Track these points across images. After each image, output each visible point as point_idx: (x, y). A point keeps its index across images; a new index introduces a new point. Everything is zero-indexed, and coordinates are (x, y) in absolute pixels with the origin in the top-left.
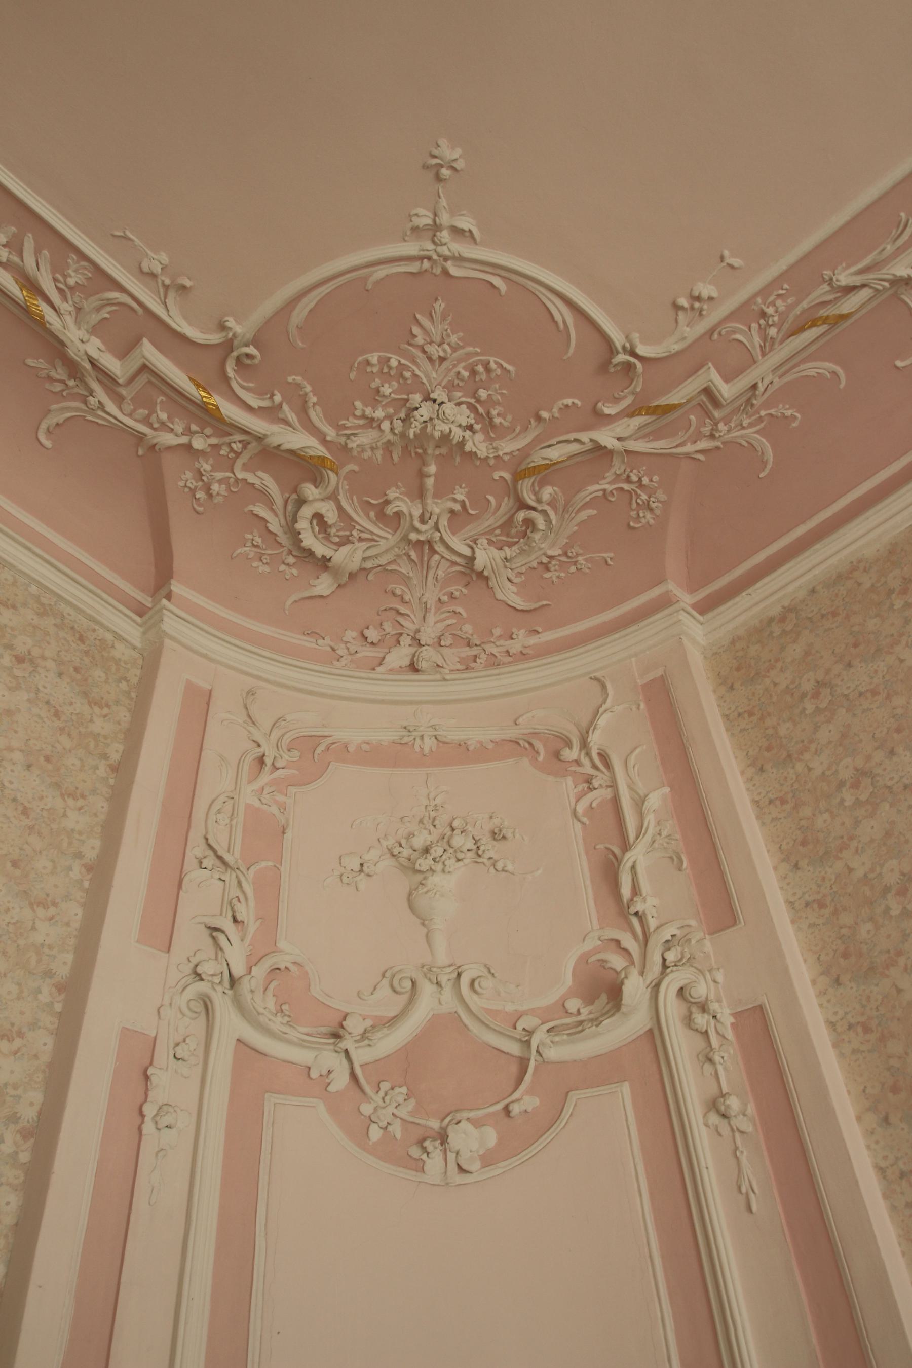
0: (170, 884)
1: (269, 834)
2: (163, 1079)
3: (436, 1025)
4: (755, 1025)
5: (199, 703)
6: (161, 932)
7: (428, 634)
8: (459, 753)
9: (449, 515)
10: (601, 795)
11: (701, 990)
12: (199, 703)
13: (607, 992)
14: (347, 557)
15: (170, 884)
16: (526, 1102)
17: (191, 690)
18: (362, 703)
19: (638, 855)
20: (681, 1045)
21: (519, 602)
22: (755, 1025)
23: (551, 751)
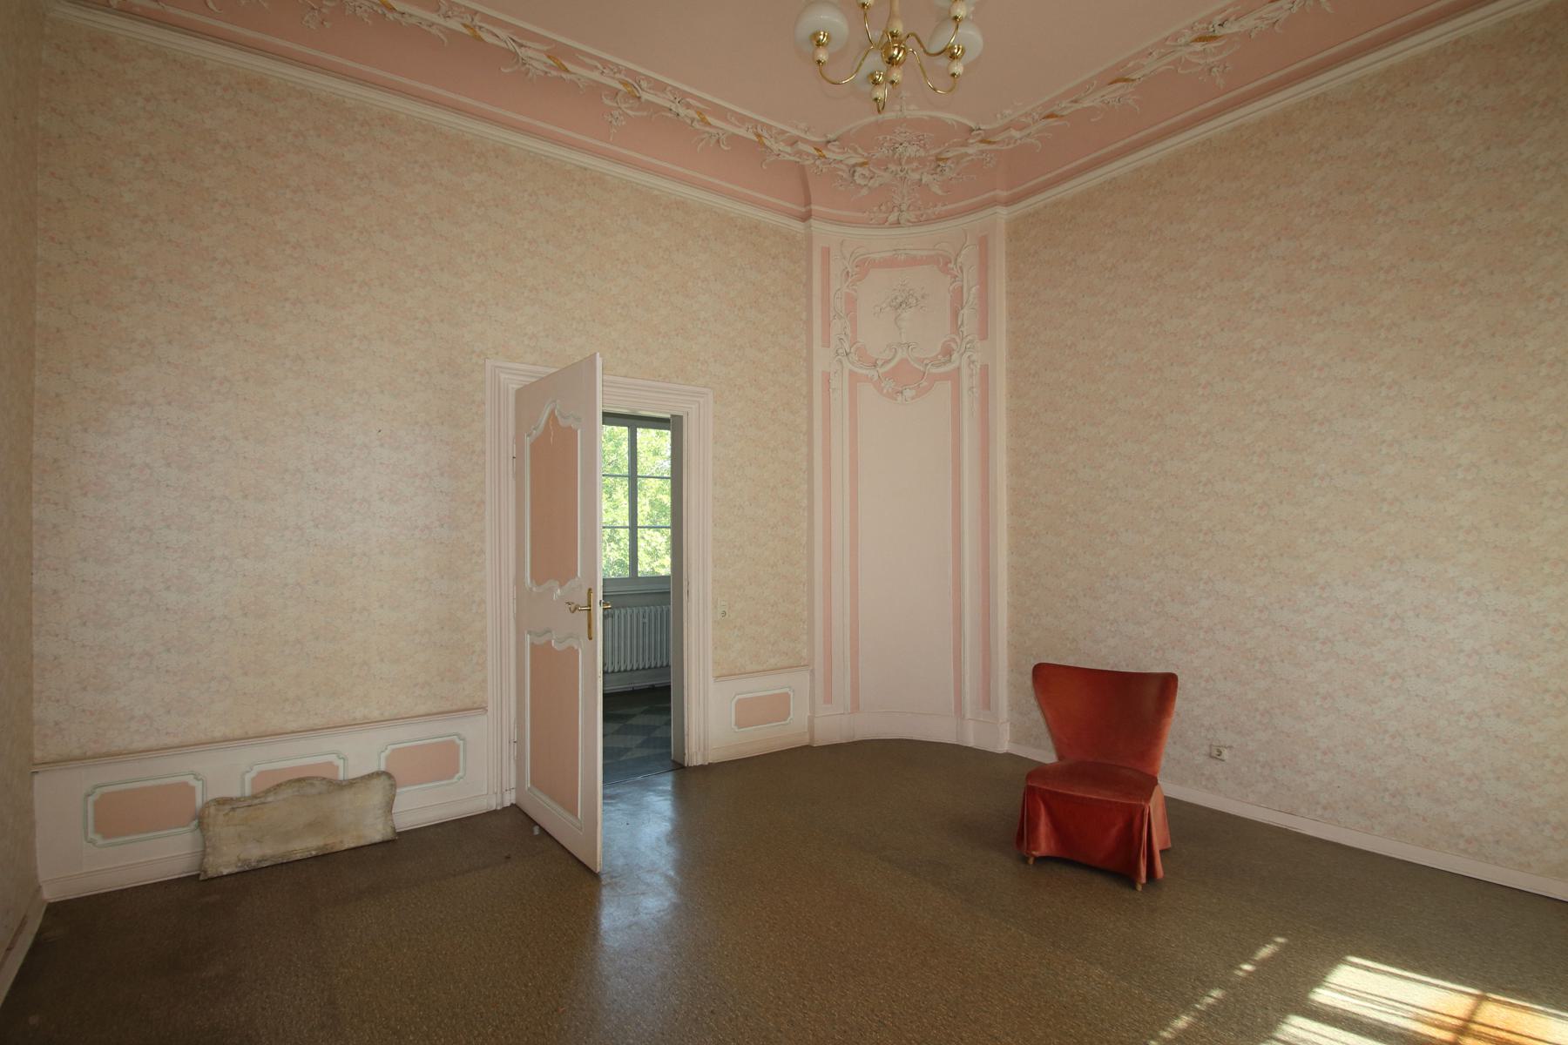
0: (827, 325)
1: (851, 302)
2: (834, 384)
3: (904, 361)
4: (985, 371)
5: (826, 252)
6: (826, 343)
7: (904, 207)
8: (913, 261)
9: (1006, 727)
10: (958, 284)
11: (974, 357)
12: (826, 252)
13: (948, 352)
14: (874, 183)
15: (827, 325)
16: (925, 384)
17: (784, 699)
18: (880, 242)
19: (965, 311)
20: (965, 372)
21: (940, 192)
22: (985, 371)
23: (944, 263)
